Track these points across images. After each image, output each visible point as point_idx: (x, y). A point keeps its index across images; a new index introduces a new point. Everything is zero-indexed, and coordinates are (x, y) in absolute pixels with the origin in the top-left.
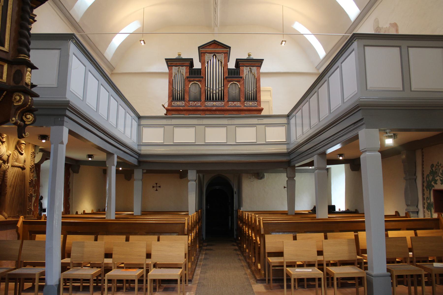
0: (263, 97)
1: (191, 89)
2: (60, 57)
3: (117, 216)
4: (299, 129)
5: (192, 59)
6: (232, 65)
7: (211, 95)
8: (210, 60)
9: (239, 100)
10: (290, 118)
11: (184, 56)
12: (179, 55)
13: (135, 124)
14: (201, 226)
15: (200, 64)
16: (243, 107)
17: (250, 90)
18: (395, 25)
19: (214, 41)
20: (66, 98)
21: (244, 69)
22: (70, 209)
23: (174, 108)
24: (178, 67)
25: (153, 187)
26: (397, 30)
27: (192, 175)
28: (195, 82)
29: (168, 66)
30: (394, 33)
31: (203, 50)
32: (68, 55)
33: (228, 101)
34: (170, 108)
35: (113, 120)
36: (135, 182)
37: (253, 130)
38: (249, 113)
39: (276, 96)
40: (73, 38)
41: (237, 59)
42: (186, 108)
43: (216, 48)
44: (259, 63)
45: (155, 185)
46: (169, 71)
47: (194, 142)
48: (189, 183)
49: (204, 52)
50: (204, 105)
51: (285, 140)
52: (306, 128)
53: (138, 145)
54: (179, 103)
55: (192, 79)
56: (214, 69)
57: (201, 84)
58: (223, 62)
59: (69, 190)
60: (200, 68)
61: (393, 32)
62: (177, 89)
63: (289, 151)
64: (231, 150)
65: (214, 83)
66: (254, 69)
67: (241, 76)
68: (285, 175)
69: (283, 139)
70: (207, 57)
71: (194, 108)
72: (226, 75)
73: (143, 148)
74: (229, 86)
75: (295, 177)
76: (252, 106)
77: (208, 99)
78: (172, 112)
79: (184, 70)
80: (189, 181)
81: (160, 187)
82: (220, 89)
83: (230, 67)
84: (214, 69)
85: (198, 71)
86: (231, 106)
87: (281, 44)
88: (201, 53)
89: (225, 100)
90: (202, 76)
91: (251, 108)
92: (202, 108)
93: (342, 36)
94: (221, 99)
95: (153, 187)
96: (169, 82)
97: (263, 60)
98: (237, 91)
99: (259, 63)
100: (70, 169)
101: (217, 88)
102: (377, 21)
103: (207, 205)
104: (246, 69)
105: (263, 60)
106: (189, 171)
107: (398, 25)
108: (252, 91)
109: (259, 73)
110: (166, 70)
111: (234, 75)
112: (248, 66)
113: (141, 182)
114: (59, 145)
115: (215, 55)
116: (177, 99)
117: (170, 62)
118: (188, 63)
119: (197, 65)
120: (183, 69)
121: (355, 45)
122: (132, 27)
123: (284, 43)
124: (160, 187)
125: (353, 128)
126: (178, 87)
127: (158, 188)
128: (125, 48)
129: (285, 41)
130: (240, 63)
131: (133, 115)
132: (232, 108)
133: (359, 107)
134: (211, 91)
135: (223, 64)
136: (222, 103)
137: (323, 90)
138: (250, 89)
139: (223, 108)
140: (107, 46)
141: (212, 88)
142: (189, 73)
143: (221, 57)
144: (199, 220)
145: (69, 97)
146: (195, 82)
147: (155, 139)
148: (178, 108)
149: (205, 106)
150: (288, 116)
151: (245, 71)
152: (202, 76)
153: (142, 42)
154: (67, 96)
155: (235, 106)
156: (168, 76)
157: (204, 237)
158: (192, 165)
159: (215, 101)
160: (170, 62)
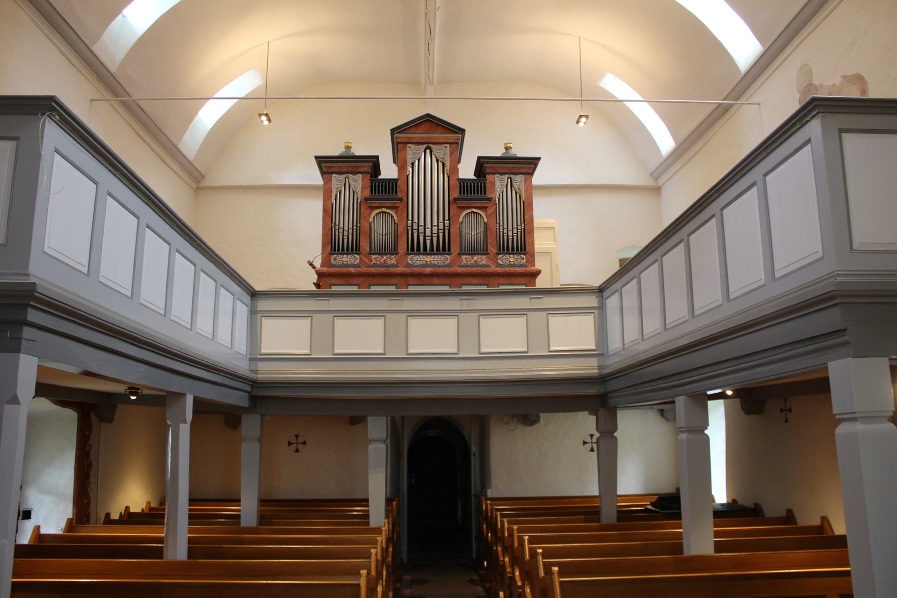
0: (541, 242)
1: (375, 227)
2: (16, 161)
3: (204, 532)
4: (631, 322)
5: (377, 157)
6: (467, 171)
7: (422, 239)
8: (419, 160)
9: (485, 252)
10: (606, 294)
11: (358, 151)
12: (348, 148)
13: (243, 310)
14: (398, 538)
15: (395, 168)
16: (493, 268)
17: (510, 228)
18: (859, 80)
19: (428, 115)
20: (28, 275)
21: (497, 179)
22: (92, 510)
23: (336, 269)
24: (344, 176)
25: (290, 444)
26: (864, 91)
27: (377, 428)
28: (384, 210)
30: (857, 96)
31: (403, 136)
32: (38, 156)
33: (460, 254)
34: (325, 269)
35: (181, 311)
36: (244, 444)
37: (518, 324)
38: (507, 280)
39: (570, 242)
40: (53, 109)
41: (479, 158)
42: (363, 269)
43: (430, 132)
44: (530, 164)
45: (293, 440)
47: (382, 351)
48: (371, 447)
49: (404, 140)
50: (404, 263)
51: (593, 347)
52: (652, 324)
53: (250, 359)
54: (346, 259)
55: (377, 203)
56: (427, 179)
57: (397, 214)
58: (448, 164)
59: (90, 465)
60: (396, 177)
61: (853, 93)
62: (341, 226)
63: (606, 371)
64: (470, 371)
65: (425, 211)
66: (519, 180)
67: (489, 195)
68: (594, 418)
69: (589, 343)
70: (411, 152)
71: (382, 270)
72: (456, 194)
73: (262, 366)
74: (461, 220)
75: (616, 429)
76: (514, 266)
77: (414, 249)
78: (328, 279)
79: (358, 182)
80: (371, 441)
81: (304, 443)
82: (441, 225)
83: (462, 175)
84: (427, 179)
85: (392, 184)
86: (466, 266)
87: (578, 122)
88: (398, 143)
89: (452, 251)
90: (399, 195)
91: (512, 269)
92: (400, 270)
93: (714, 106)
94: (445, 249)
95: (290, 444)
96: (325, 210)
97: (539, 159)
98: (481, 229)
99: (530, 164)
100: (92, 414)
101: (435, 223)
102: (806, 70)
103: (409, 476)
104: (501, 181)
105: (539, 159)
106: (370, 420)
107: (867, 79)
108: (515, 231)
109: (530, 188)
110: (319, 180)
111: (472, 193)
113: (258, 444)
114: (6, 407)
115: (430, 149)
116: (343, 250)
117: (327, 165)
118: (367, 167)
119: (388, 171)
120: (356, 181)
121: (814, 128)
122: (244, 84)
123: (583, 120)
124: (304, 443)
126: (345, 223)
127: (300, 447)
128: (228, 131)
129: (587, 117)
131: (236, 288)
132: (469, 270)
133: (833, 297)
134: (421, 229)
135: (447, 168)
136: (446, 259)
137: (704, 238)
138: (510, 227)
139: (447, 270)
140: (187, 127)
141: (422, 223)
143: (443, 152)
144: (395, 525)
145: (39, 274)
146: (384, 210)
147: (289, 344)
148: (345, 270)
149: (408, 265)
150: (601, 291)
151: (499, 184)
152: (399, 195)
153: (264, 118)
154: (31, 270)
155: (476, 265)
156: (321, 193)
158: (379, 405)
159: (430, 254)
160: (327, 165)
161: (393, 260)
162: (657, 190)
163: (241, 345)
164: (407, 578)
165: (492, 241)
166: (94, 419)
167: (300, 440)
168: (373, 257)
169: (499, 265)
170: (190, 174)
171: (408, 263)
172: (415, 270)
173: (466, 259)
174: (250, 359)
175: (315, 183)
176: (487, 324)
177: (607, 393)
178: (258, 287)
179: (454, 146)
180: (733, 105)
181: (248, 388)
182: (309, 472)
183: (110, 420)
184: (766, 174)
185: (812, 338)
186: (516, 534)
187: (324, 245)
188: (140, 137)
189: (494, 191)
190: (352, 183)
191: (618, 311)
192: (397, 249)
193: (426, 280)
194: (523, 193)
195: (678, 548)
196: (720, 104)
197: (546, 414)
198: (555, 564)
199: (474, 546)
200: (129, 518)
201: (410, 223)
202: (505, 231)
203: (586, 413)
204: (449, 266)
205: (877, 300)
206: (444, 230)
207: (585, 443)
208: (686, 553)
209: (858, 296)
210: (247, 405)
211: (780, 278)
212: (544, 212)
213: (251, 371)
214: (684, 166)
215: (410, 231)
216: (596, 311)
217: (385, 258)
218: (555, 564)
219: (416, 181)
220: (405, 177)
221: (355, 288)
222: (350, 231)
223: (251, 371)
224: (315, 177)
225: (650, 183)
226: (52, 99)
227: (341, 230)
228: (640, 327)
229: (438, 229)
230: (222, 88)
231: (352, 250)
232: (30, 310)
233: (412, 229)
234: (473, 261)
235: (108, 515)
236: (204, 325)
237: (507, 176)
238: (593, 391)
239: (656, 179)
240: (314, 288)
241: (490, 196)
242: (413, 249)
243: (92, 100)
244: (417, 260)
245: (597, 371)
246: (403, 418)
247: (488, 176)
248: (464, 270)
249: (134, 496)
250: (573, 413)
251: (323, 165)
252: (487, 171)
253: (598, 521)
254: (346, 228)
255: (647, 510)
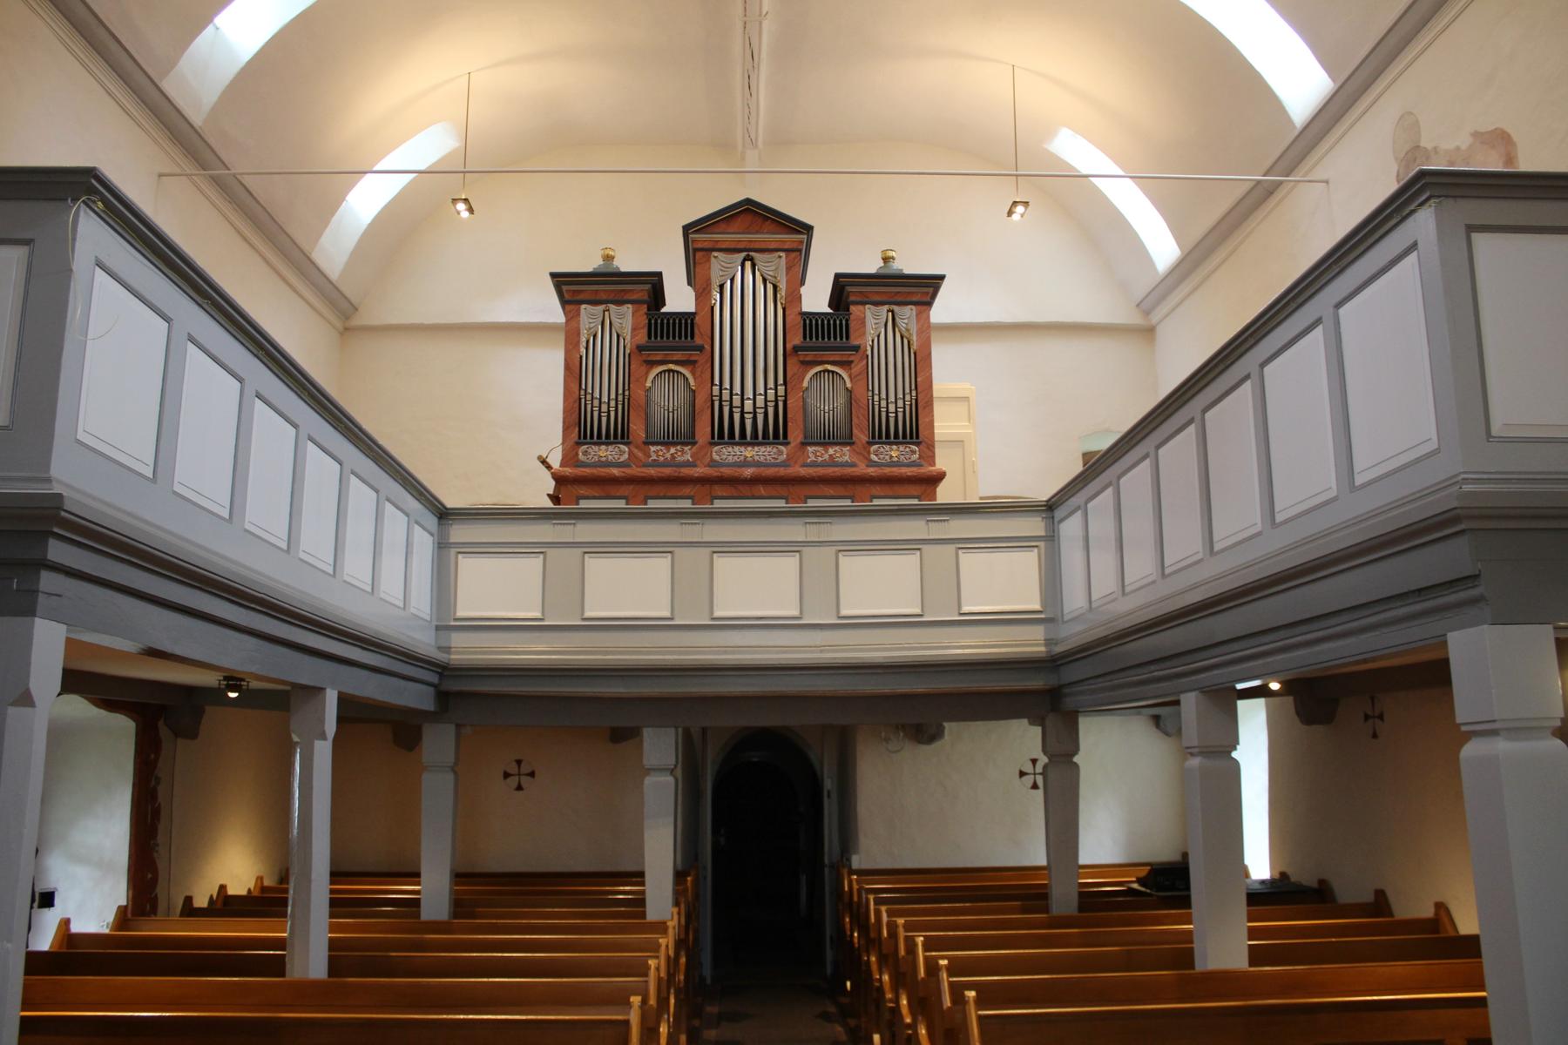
0: (945, 424)
1: (656, 396)
2: (28, 281)
4: (1103, 563)
5: (659, 275)
6: (816, 298)
7: (737, 417)
8: (732, 280)
9: (848, 440)
10: (1059, 514)
11: (626, 264)
12: (608, 258)
13: (424, 543)
14: (696, 939)
15: (690, 294)
16: (862, 469)
17: (892, 399)
18: (1501, 139)
19: (748, 201)
20: (49, 480)
21: (868, 314)
23: (588, 471)
24: (602, 307)
25: (506, 775)
26: (1510, 160)
27: (659, 748)
28: (672, 366)
29: (564, 303)
30: (1498, 167)
31: (704, 238)
32: (66, 272)
33: (804, 444)
34: (568, 471)
35: (316, 543)
36: (426, 777)
37: (906, 565)
38: (887, 490)
39: (997, 423)
40: (92, 191)
41: (838, 276)
42: (635, 471)
43: (752, 230)
44: (926, 287)
45: (513, 769)
46: (567, 321)
47: (667, 614)
48: (648, 781)
49: (706, 245)
50: (707, 460)
51: (1037, 607)
53: (438, 628)
54: (605, 452)
55: (659, 356)
56: (747, 312)
57: (693, 374)
58: (783, 286)
59: (156, 813)
60: (693, 310)
61: (1492, 163)
62: (597, 395)
63: (1059, 649)
64: (821, 648)
65: (742, 368)
66: (907, 314)
67: (854, 342)
68: (1038, 730)
69: (1029, 599)
70: (719, 266)
71: (667, 471)
72: (796, 339)
73: (458, 640)
74: (805, 384)
75: (1076, 750)
76: (898, 464)
77: (724, 435)
78: (573, 487)
79: (626, 319)
80: (648, 771)
81: (532, 774)
82: (771, 393)
83: (808, 306)
84: (747, 312)
85: (685, 322)
86: (814, 464)
87: (1010, 213)
88: (696, 250)
89: (790, 438)
90: (698, 341)
91: (896, 471)
92: (699, 471)
93: (1252, 184)
94: (777, 435)
95: (506, 775)
96: (567, 367)
97: (942, 278)
98: (841, 401)
99: (926, 287)
100: (161, 723)
102: (1409, 123)
103: (715, 832)
104: (876, 316)
105: (942, 278)
106: (647, 733)
107: (1515, 138)
108: (900, 403)
109: (926, 328)
110: (557, 315)
111: (824, 337)
112: (882, 304)
113: (451, 777)
114: (12, 711)
115: (752, 260)
116: (599, 436)
117: (571, 288)
118: (642, 291)
119: (679, 298)
121: (1424, 223)
122: (427, 147)
123: (1020, 209)
124: (532, 774)
125: (1418, 607)
126: (603, 389)
127: (525, 781)
128: (399, 230)
129: (1026, 204)
130: (849, 289)
131: (413, 504)
132: (821, 471)
133: (1456, 520)
134: (737, 400)
135: (782, 293)
136: (780, 453)
137: (1231, 415)
138: (892, 396)
139: (782, 471)
140: (326, 223)
141: (737, 389)
142: (645, 331)
143: (775, 265)
144: (690, 918)
145: (69, 479)
146: (672, 366)
147: (505, 601)
148: (603, 471)
149: (713, 464)
150: (1050, 508)
151: (872, 322)
152: (698, 341)
153: (461, 206)
154: (55, 472)
155: (832, 462)
156: (561, 338)
157: (707, 972)
158: (663, 708)
159: (752, 444)
160: (571, 288)
161: (687, 454)
162: (1148, 332)
163: (422, 603)
164: (712, 1009)
165: (860, 421)
166: (164, 731)
167: (525, 769)
168: (653, 448)
169: (871, 464)
170: (332, 304)
171: (712, 460)
172: (726, 471)
173: (815, 453)
174: (438, 628)
175: (551, 320)
176: (852, 566)
177: (1061, 687)
178: (451, 502)
179: (794, 255)
180: (1281, 183)
181: (434, 679)
182: (539, 826)
183: (193, 735)
184: (1339, 305)
185: (1420, 590)
186: (902, 934)
187: (566, 429)
188: (245, 239)
189: (864, 334)
190: (615, 320)
191: (1081, 543)
192: (693, 435)
193: (745, 490)
194: (915, 338)
195: (1184, 958)
196: (1259, 182)
197: (954, 724)
198: (970, 986)
199: (829, 955)
200: (226, 905)
201: (716, 390)
202: (883, 404)
203: (1025, 721)
204: (784, 464)
205: (1534, 524)
206: (776, 401)
207: (1022, 774)
208: (1200, 967)
209: (1499, 517)
210: (432, 708)
211: (1364, 486)
212: (950, 371)
213: (439, 648)
214: (1195, 289)
215: (717, 404)
216: (1042, 544)
217: (673, 450)
218: (970, 986)
219: (726, 317)
220: (707, 309)
221: (621, 504)
222: (613, 403)
223: (439, 648)
224: (554, 312)
225: (1136, 319)
226: (91, 172)
227: (596, 403)
228: (1118, 572)
229: (766, 401)
230: (388, 153)
231: (616, 437)
232: (52, 542)
233: (721, 401)
234: (826, 457)
235: (189, 900)
236: (357, 568)
237: (886, 308)
238: (1037, 682)
239: (1147, 313)
240: (549, 504)
241: (856, 343)
242: (721, 436)
243: (160, 175)
244: (729, 454)
245: (1043, 649)
246: (704, 730)
247: (852, 308)
248: (811, 471)
249: (234, 866)
250: (1002, 722)
251: (564, 288)
252: (852, 298)
253: (1046, 910)
254: (605, 399)
255: (1131, 892)
